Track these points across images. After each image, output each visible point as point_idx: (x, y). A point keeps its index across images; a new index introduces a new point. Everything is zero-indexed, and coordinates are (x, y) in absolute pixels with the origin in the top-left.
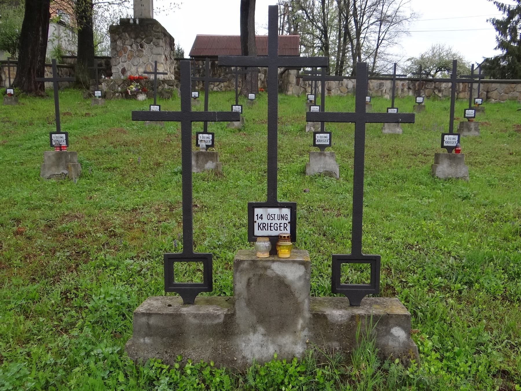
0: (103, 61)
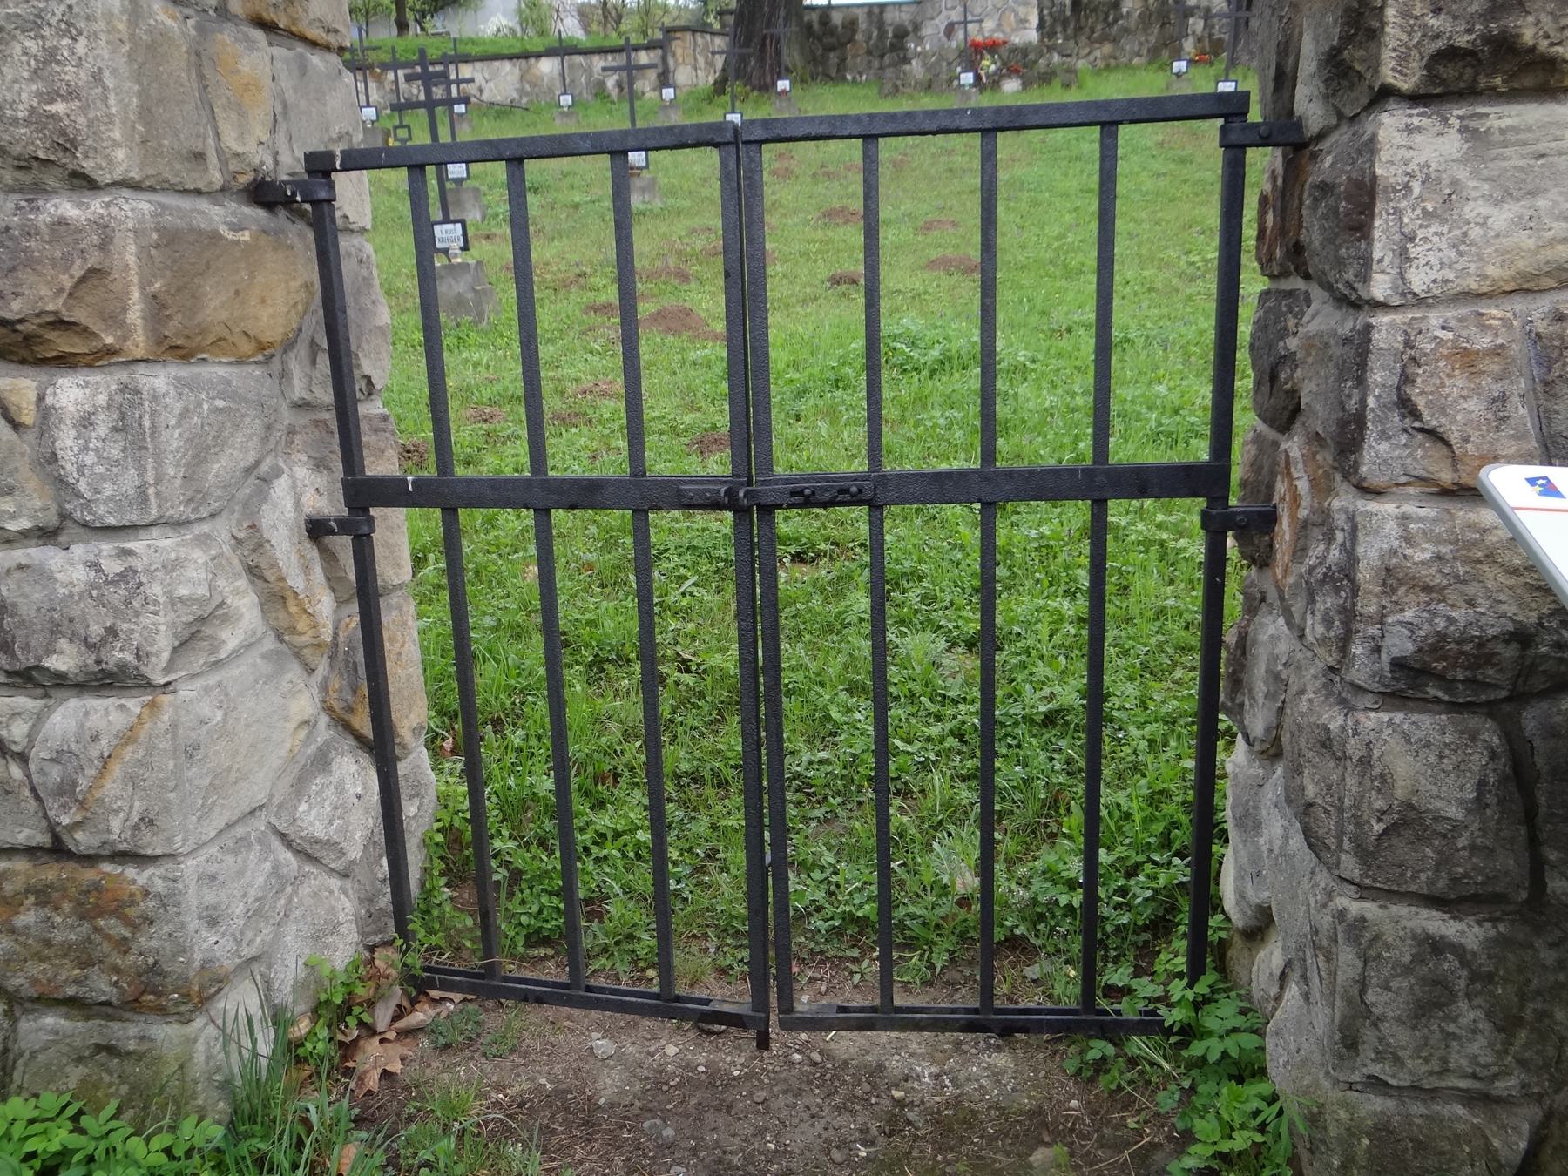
0: (815, 17)
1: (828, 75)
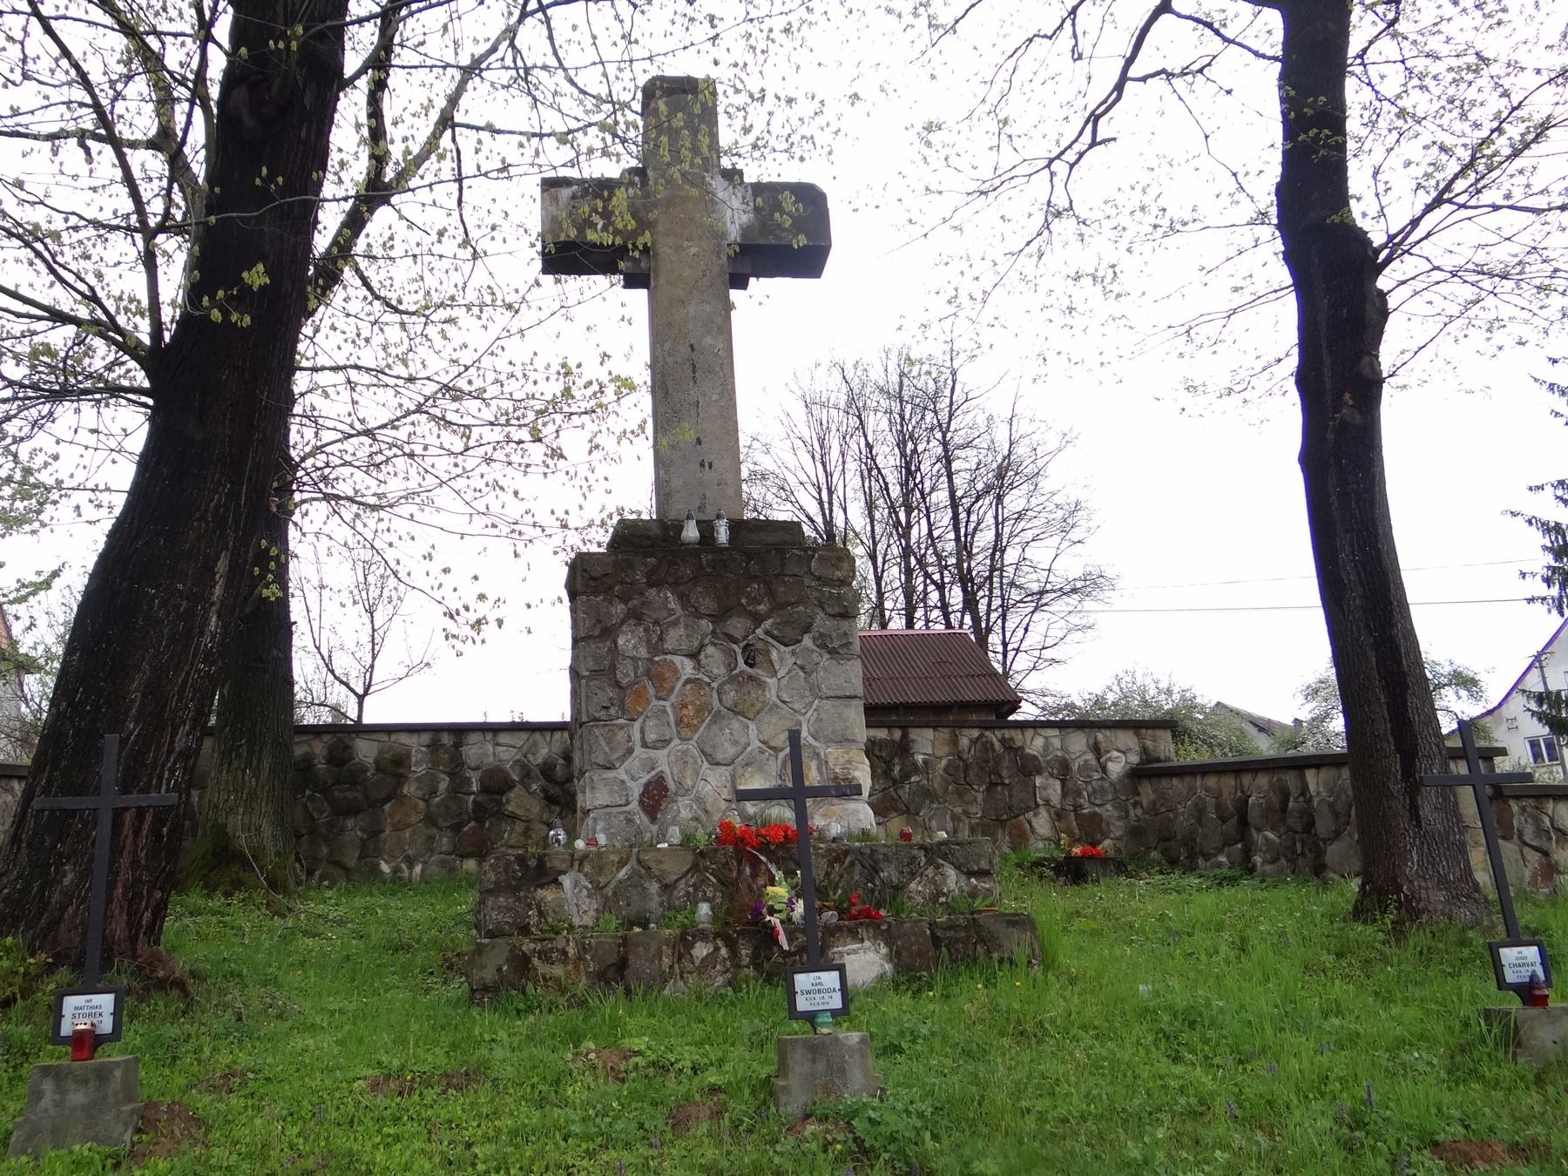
0: (319, 748)
1: (338, 864)
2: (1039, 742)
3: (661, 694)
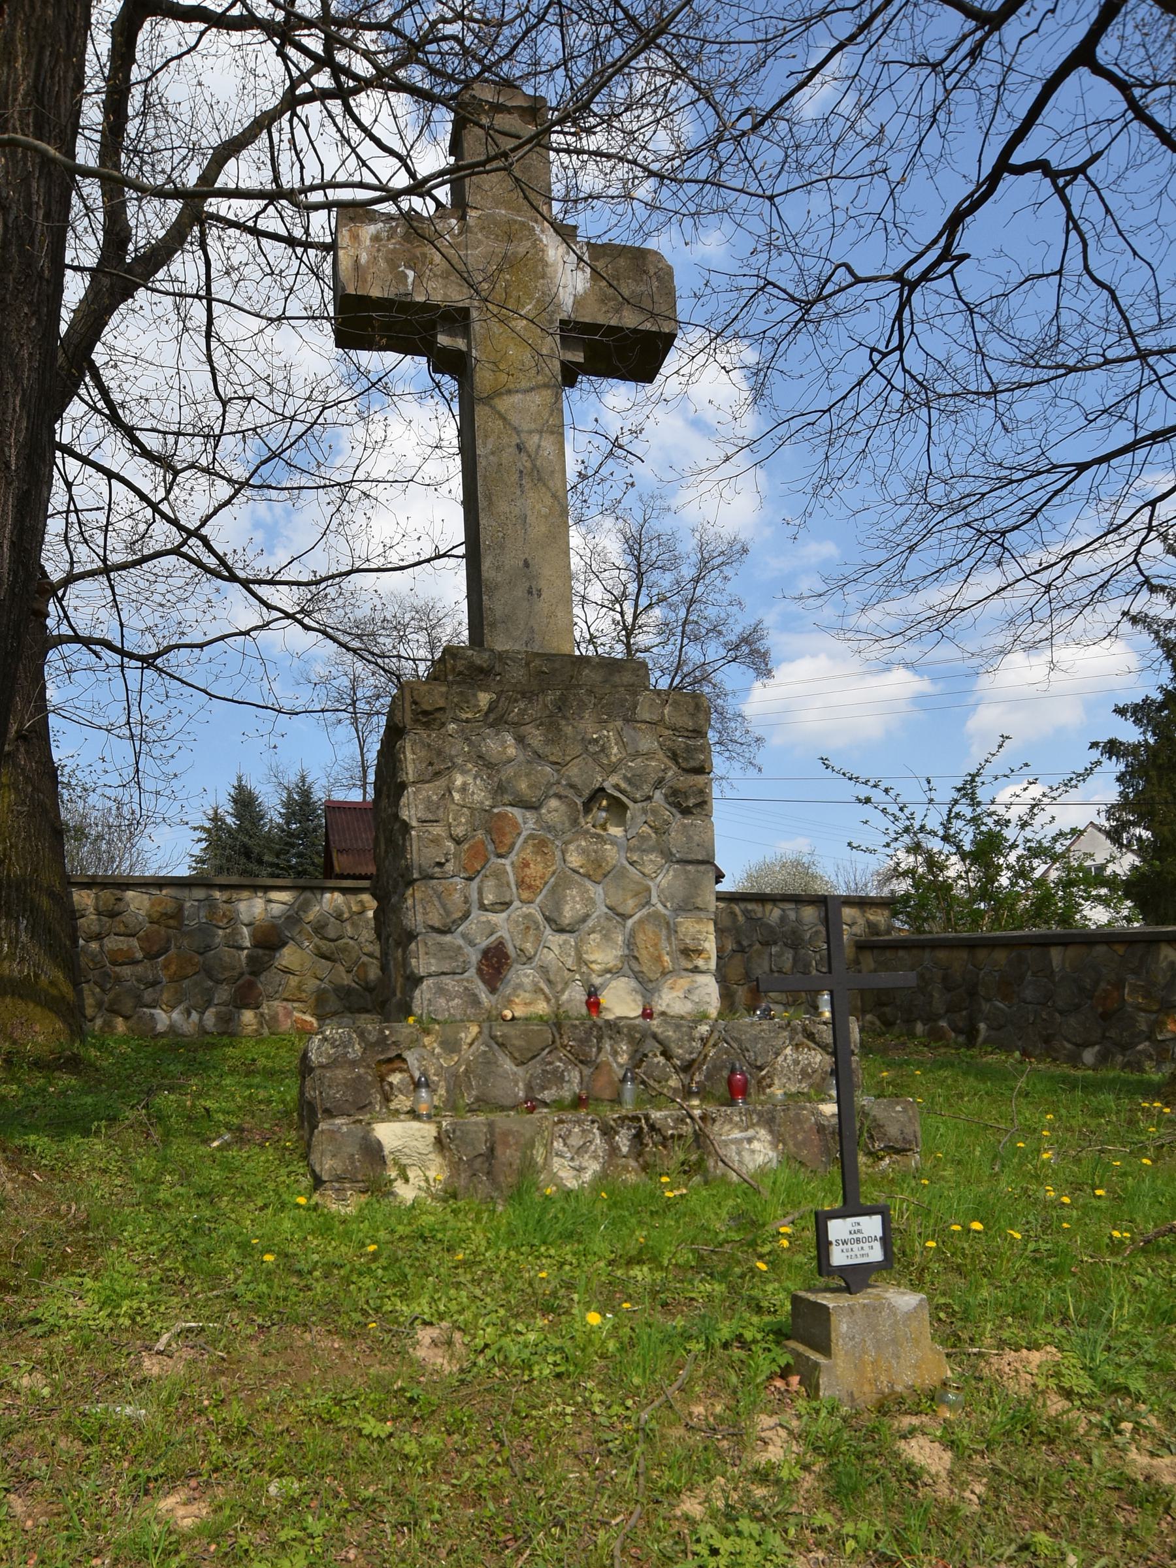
2: (777, 913)
3: (502, 851)
